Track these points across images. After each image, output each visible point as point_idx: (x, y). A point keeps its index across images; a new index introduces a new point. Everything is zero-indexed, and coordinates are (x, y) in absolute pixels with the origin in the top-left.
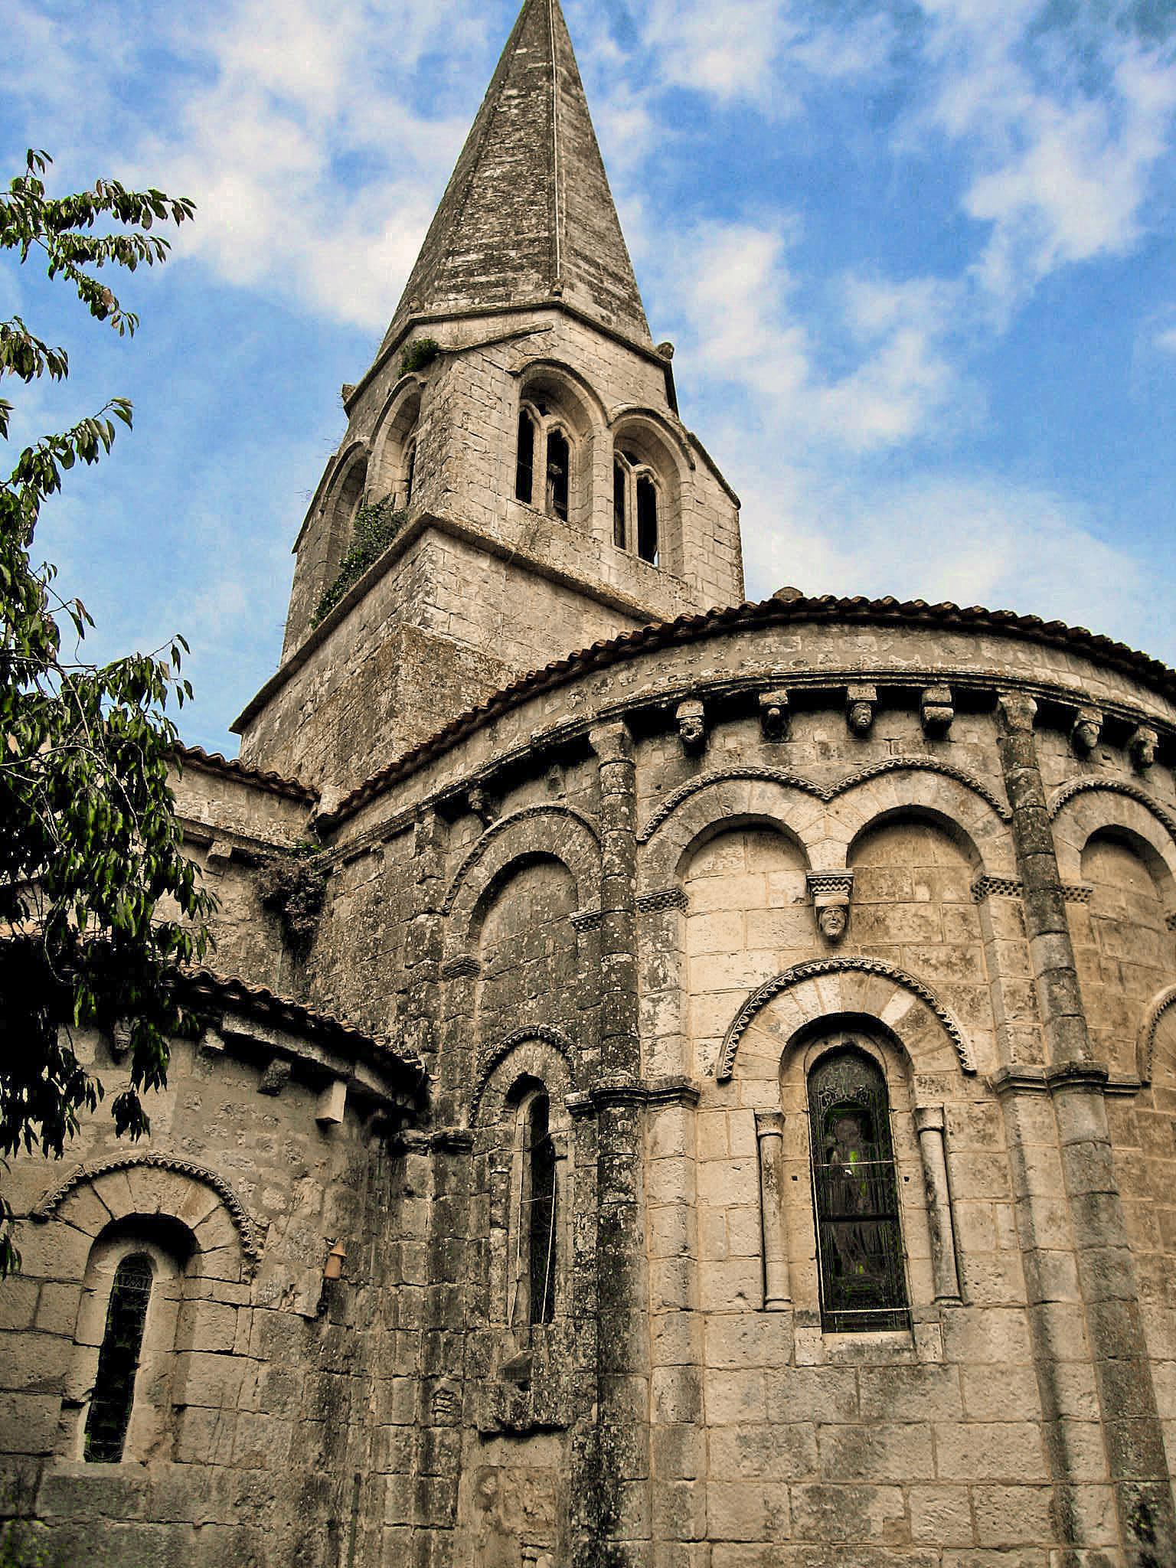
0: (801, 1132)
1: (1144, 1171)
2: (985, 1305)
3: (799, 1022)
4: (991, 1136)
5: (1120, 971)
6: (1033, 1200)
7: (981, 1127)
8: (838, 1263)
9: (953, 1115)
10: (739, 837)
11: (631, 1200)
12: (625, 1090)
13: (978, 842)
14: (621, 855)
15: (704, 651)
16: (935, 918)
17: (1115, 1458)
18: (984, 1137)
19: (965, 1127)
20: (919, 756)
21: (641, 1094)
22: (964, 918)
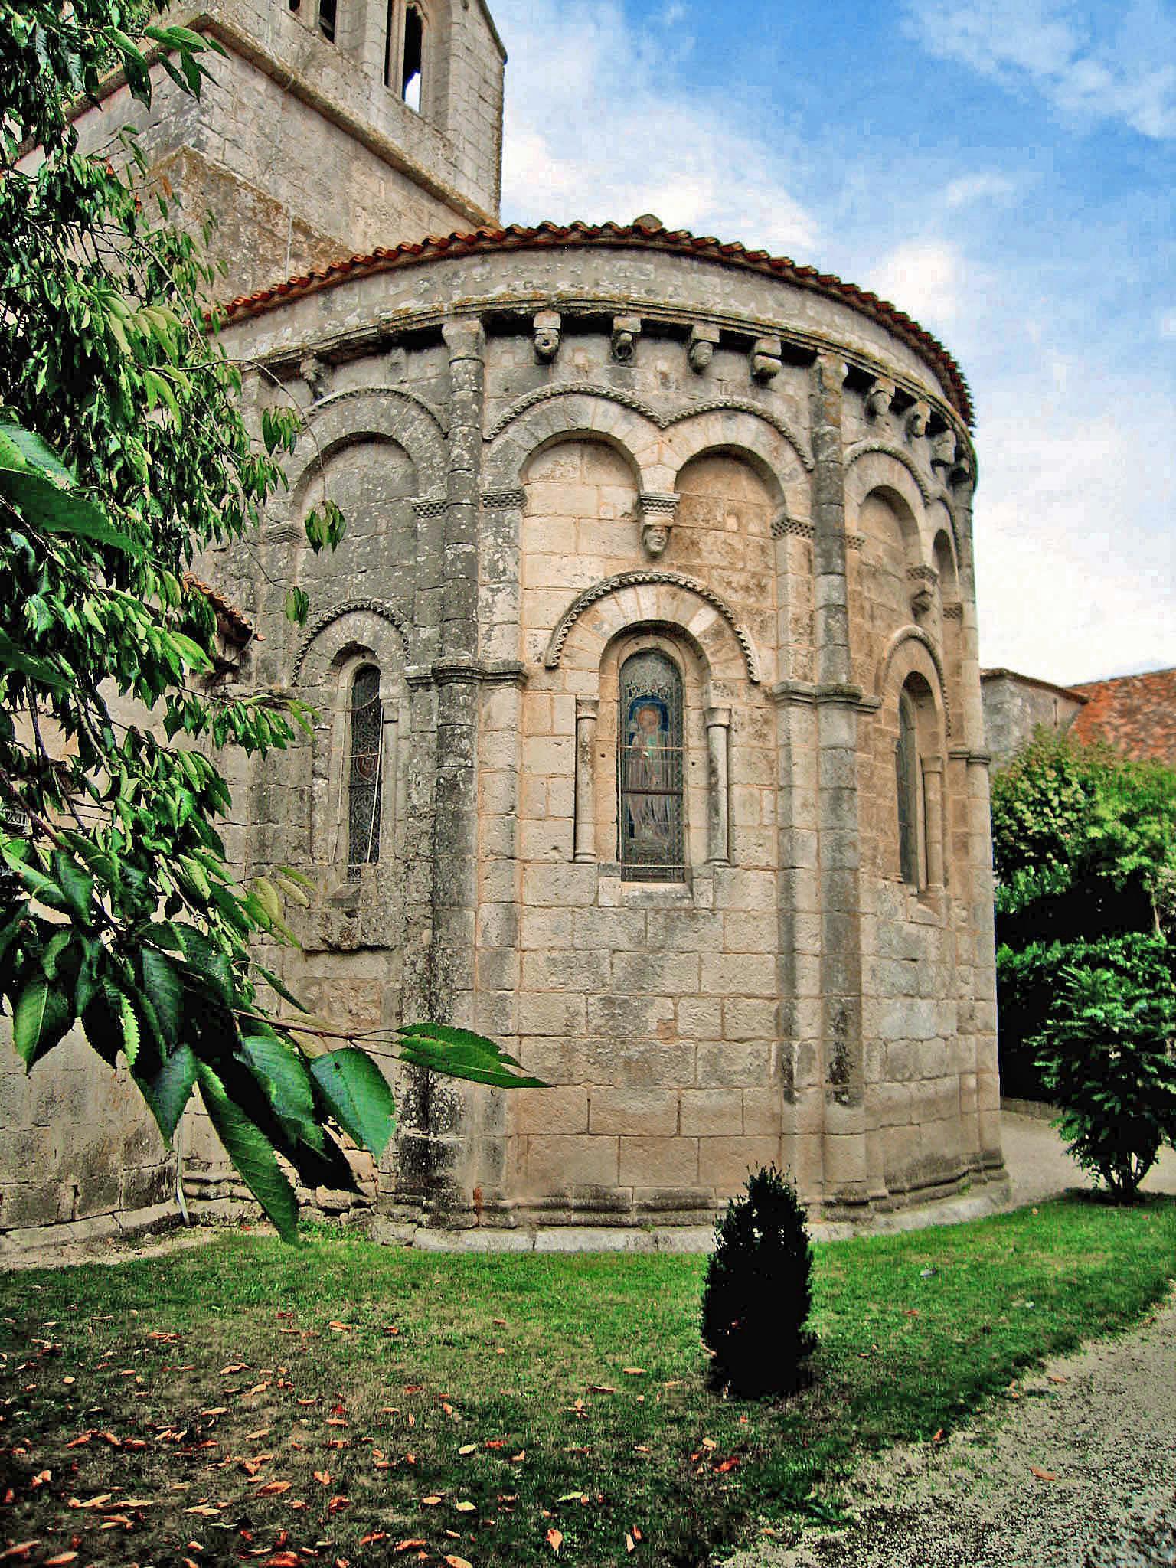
1: (872, 773)
3: (621, 623)
8: (632, 828)
12: (469, 669)
13: (784, 485)
15: (561, 261)
16: (740, 547)
17: (826, 980)
20: (745, 400)
21: (478, 673)
22: (763, 550)
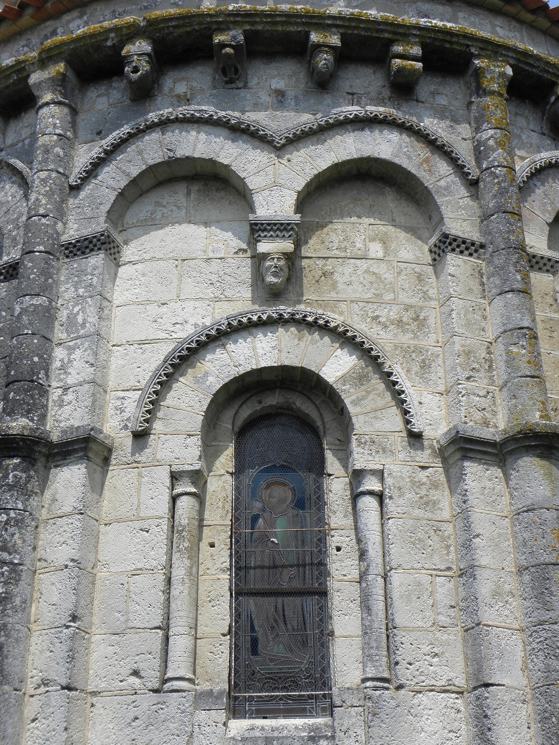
0: (224, 494)
2: (417, 688)
4: (435, 503)
6: (478, 572)
7: (423, 492)
8: (254, 642)
10: (181, 188)
11: (16, 561)
13: (439, 200)
16: (389, 276)
18: (427, 503)
22: (420, 278)
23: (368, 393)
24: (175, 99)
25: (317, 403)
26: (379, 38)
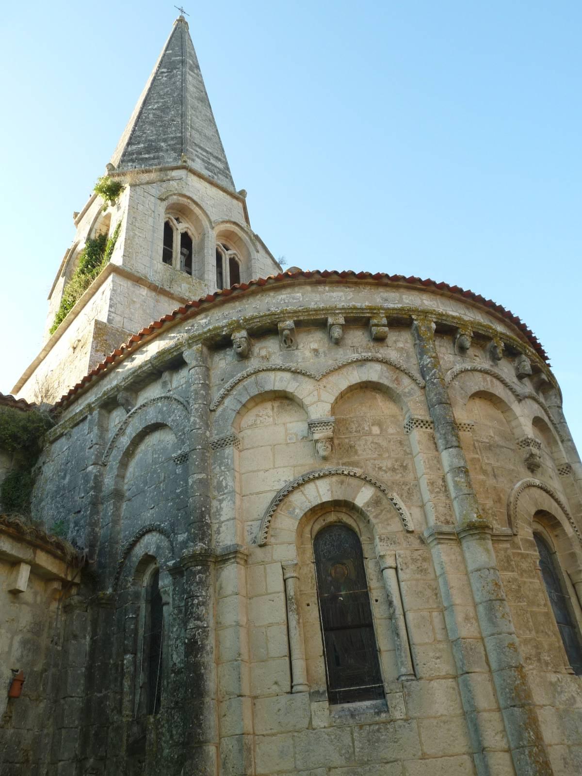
0: (311, 575)
1: (520, 587)
2: (430, 678)
4: (426, 570)
5: (494, 472)
7: (419, 565)
9: (402, 558)
11: (205, 625)
14: (201, 417)
16: (384, 444)
18: (421, 571)
19: (410, 566)
20: (370, 354)
22: (401, 443)
23: (382, 511)
24: (261, 359)
25: (355, 518)
26: (364, 317)
